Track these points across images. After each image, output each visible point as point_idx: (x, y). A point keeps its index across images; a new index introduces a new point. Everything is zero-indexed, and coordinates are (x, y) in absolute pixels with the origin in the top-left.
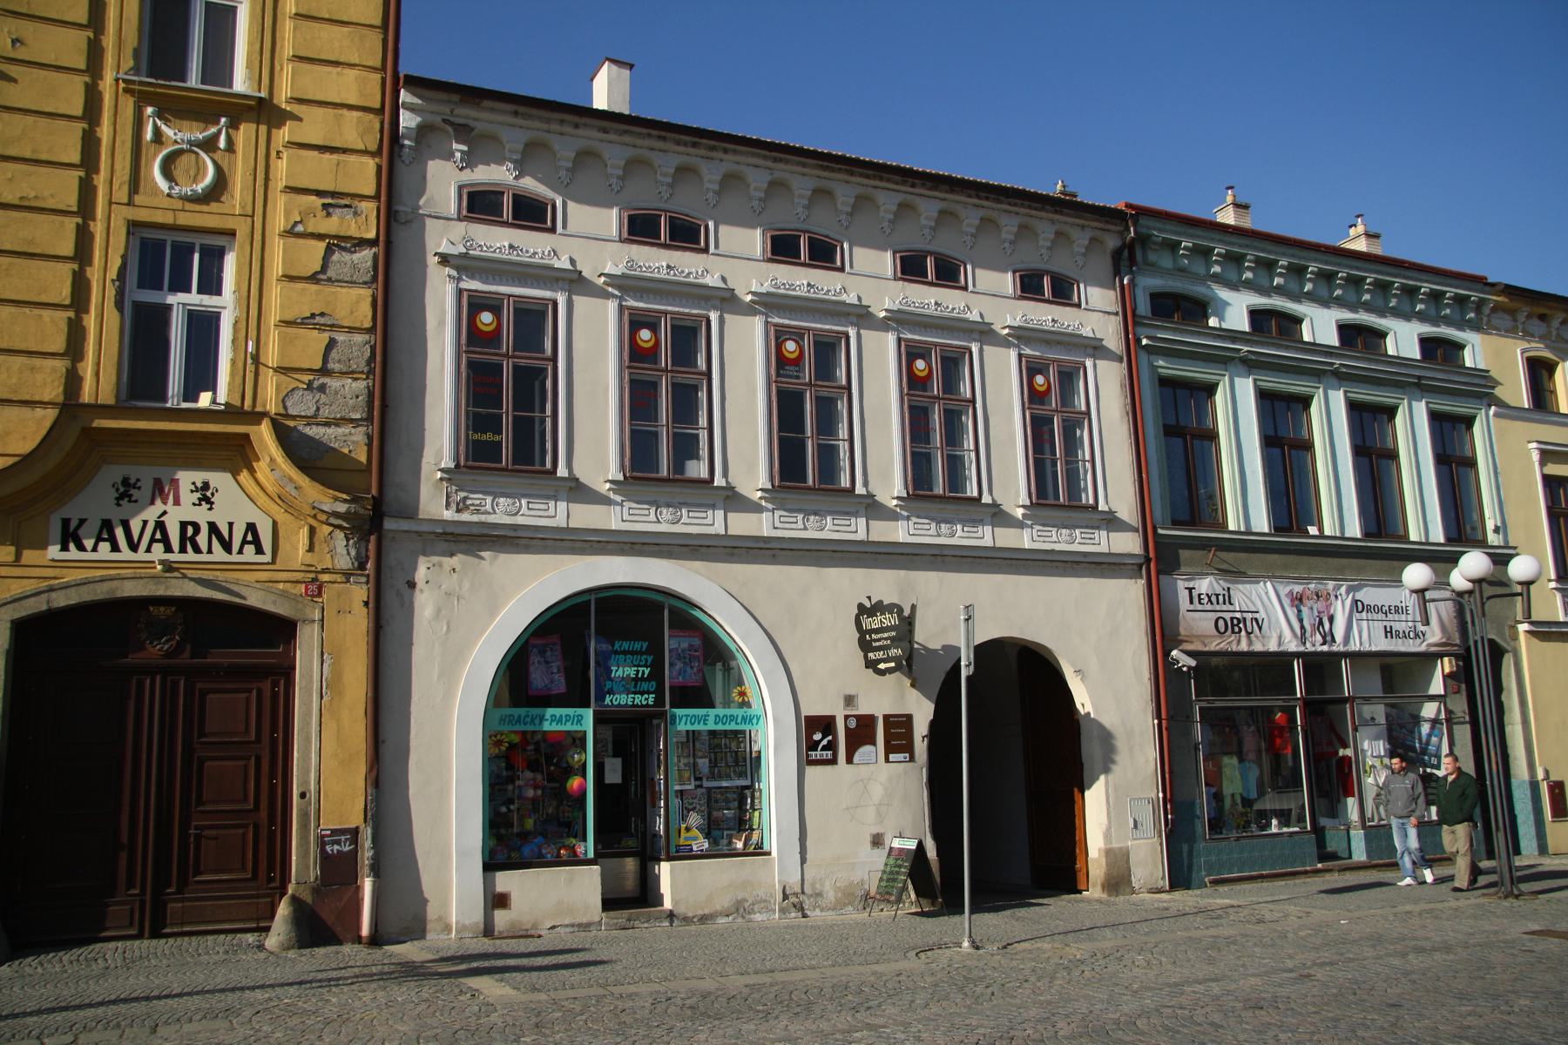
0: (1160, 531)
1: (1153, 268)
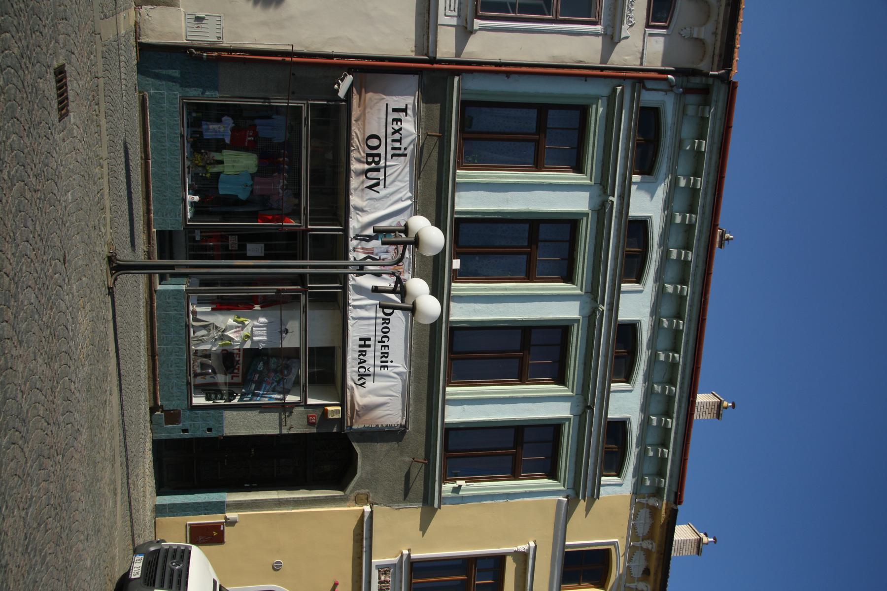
0: (456, 79)
1: (681, 112)
